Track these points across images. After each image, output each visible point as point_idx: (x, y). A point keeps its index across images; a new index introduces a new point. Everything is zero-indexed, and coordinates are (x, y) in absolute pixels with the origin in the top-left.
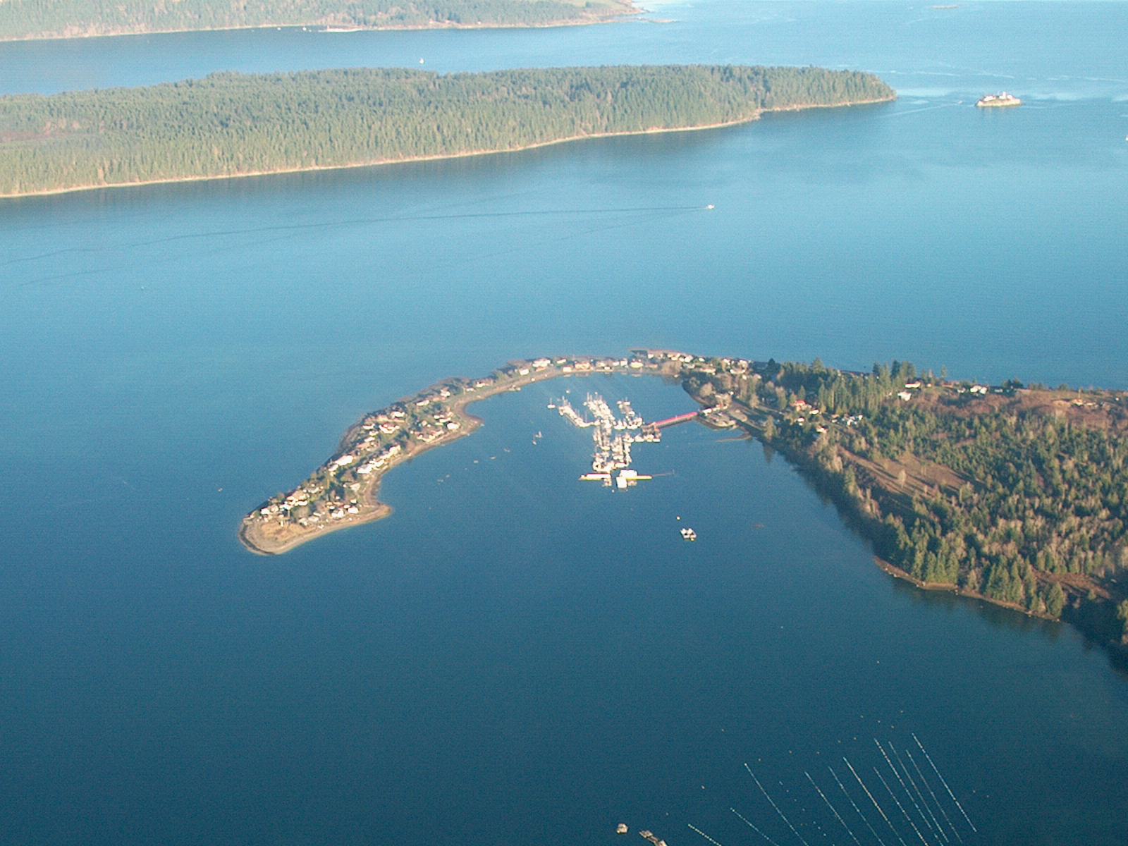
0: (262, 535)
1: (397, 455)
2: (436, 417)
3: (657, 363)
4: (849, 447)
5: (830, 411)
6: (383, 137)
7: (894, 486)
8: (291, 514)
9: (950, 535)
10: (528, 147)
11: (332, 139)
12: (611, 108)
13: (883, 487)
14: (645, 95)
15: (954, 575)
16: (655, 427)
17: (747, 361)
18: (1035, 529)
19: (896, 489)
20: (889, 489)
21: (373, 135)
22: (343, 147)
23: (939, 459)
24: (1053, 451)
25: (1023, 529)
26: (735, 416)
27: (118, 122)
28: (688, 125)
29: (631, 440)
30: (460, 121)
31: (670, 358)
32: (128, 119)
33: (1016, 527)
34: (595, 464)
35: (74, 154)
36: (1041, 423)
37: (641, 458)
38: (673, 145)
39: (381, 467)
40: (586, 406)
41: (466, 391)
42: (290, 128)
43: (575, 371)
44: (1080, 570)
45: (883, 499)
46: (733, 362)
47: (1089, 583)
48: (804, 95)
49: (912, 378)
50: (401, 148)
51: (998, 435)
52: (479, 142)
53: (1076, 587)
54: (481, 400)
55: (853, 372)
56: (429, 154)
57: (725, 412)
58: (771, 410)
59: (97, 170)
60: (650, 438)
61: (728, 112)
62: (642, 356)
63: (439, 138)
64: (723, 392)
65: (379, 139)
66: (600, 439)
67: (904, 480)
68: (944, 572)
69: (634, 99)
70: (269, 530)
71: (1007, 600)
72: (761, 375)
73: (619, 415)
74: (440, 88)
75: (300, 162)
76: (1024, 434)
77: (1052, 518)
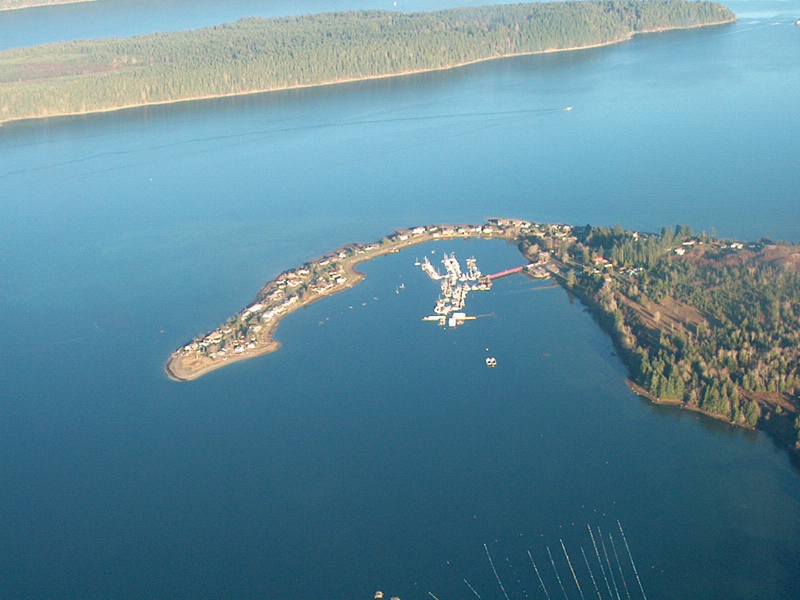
0: (181, 365)
1: (295, 303)
2: (331, 274)
3: (503, 229)
4: (626, 293)
5: (620, 264)
6: (347, 62)
7: (652, 323)
8: (206, 350)
9: (681, 362)
10: (455, 66)
11: (310, 65)
12: (518, 35)
13: (643, 324)
14: (544, 24)
15: (681, 393)
16: (488, 279)
17: (570, 227)
18: (747, 357)
19: (652, 325)
20: (647, 325)
21: (340, 61)
22: (318, 70)
23: (690, 302)
24: (779, 294)
25: (738, 357)
26: (550, 269)
27: (163, 57)
28: (576, 46)
29: (469, 289)
30: (404, 48)
31: (514, 225)
32: (170, 55)
33: (732, 356)
34: (437, 308)
35: (124, 82)
36: (774, 272)
37: (473, 303)
38: (563, 61)
39: (281, 313)
40: (443, 263)
41: (357, 253)
42: (280, 58)
43: (442, 236)
44: (776, 389)
45: (641, 334)
46: (560, 227)
47: (782, 399)
48: (666, 20)
49: (689, 237)
50: (361, 70)
51: (740, 282)
52: (419, 63)
53: (770, 402)
54: (368, 260)
55: (647, 233)
56: (381, 73)
57: (543, 266)
58: (577, 264)
59: (141, 93)
60: (483, 287)
61: (606, 34)
62: (494, 224)
63: (388, 62)
64: (544, 251)
65: (344, 64)
66: (446, 288)
67: (658, 319)
68: (673, 391)
69: (535, 28)
70: (186, 362)
71: (718, 413)
72: (577, 237)
73: (464, 269)
74: (396, 25)
75: (287, 82)
76: (760, 281)
77: (761, 347)
